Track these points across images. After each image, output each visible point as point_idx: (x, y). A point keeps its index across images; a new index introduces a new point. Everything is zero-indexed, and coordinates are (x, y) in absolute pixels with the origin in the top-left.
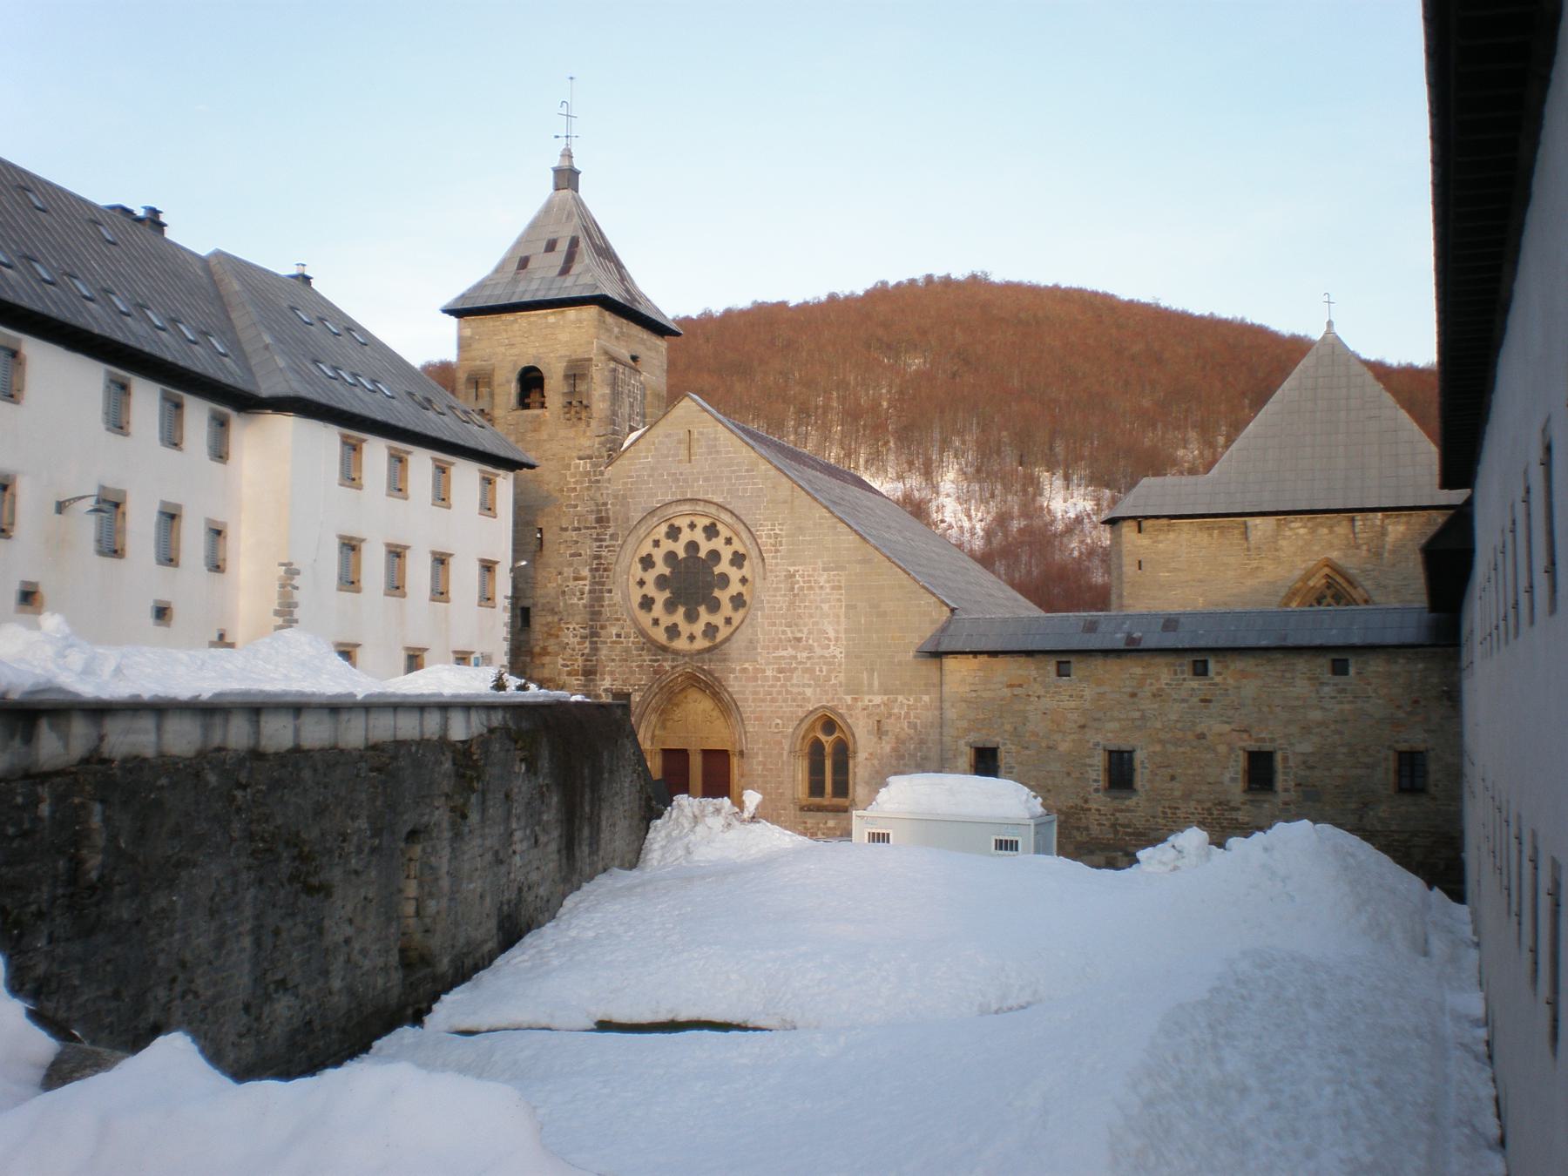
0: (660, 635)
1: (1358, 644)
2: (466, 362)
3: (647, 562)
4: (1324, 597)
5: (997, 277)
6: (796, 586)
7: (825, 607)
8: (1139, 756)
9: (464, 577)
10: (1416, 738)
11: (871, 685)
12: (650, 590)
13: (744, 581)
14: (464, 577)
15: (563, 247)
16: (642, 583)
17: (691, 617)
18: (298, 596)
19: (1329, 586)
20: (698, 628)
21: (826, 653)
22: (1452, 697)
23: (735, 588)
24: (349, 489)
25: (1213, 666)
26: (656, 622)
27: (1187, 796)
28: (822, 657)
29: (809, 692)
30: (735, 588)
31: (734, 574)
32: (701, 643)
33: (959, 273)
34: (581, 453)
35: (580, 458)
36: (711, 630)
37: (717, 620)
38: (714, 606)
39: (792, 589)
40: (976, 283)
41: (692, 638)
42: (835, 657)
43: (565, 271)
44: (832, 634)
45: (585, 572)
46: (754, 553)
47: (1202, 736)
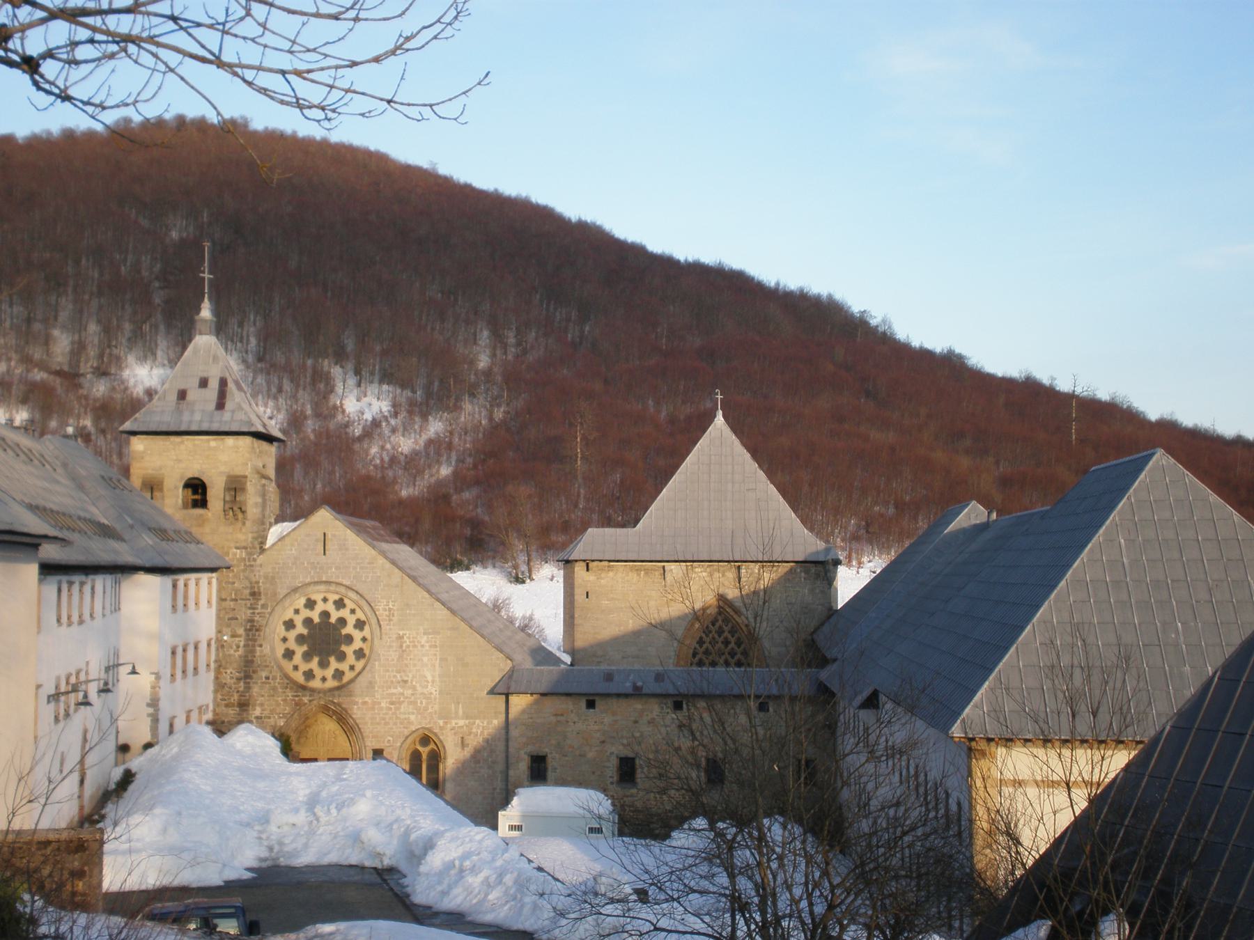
4: (717, 621)
6: (404, 645)
7: (425, 659)
11: (457, 713)
13: (364, 639)
15: (214, 384)
19: (720, 613)
21: (425, 691)
23: (357, 644)
28: (422, 693)
29: (412, 717)
30: (357, 644)
31: (357, 635)
32: (331, 683)
34: (238, 545)
35: (237, 548)
39: (401, 646)
42: (431, 693)
44: (430, 678)
46: (374, 621)
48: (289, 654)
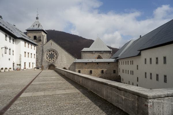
0: (49, 61)
1: (21, 40)
2: (138, 41)
3: (47, 54)
5: (56, 30)
8: (92, 71)
9: (33, 55)
10: (115, 69)
12: (48, 57)
14: (33, 55)
15: (38, 25)
16: (47, 56)
17: (52, 59)
18: (21, 58)
20: (52, 60)
22: (118, 66)
24: (87, 101)
26: (52, 61)
27: (96, 74)
32: (53, 62)
33: (53, 30)
36: (53, 60)
37: (54, 59)
38: (54, 58)
40: (54, 31)
41: (52, 61)
43: (38, 27)
45: (41, 55)
48: (50, 60)
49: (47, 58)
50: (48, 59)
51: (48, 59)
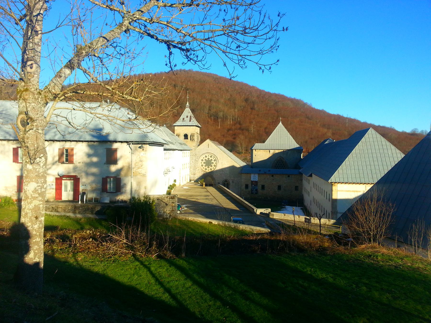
3: (202, 160)
12: (203, 164)
25: (274, 176)
29: (224, 177)
47: (273, 184)
49: (202, 165)
50: (204, 166)
51: (204, 166)
